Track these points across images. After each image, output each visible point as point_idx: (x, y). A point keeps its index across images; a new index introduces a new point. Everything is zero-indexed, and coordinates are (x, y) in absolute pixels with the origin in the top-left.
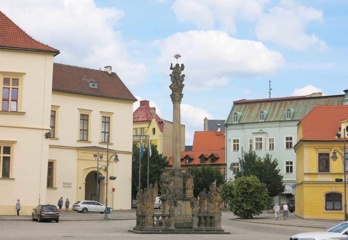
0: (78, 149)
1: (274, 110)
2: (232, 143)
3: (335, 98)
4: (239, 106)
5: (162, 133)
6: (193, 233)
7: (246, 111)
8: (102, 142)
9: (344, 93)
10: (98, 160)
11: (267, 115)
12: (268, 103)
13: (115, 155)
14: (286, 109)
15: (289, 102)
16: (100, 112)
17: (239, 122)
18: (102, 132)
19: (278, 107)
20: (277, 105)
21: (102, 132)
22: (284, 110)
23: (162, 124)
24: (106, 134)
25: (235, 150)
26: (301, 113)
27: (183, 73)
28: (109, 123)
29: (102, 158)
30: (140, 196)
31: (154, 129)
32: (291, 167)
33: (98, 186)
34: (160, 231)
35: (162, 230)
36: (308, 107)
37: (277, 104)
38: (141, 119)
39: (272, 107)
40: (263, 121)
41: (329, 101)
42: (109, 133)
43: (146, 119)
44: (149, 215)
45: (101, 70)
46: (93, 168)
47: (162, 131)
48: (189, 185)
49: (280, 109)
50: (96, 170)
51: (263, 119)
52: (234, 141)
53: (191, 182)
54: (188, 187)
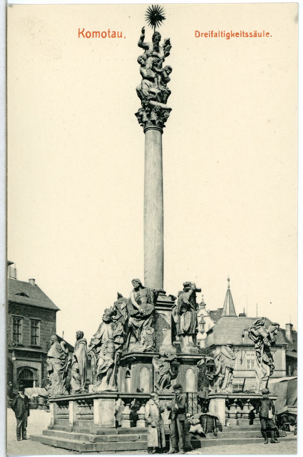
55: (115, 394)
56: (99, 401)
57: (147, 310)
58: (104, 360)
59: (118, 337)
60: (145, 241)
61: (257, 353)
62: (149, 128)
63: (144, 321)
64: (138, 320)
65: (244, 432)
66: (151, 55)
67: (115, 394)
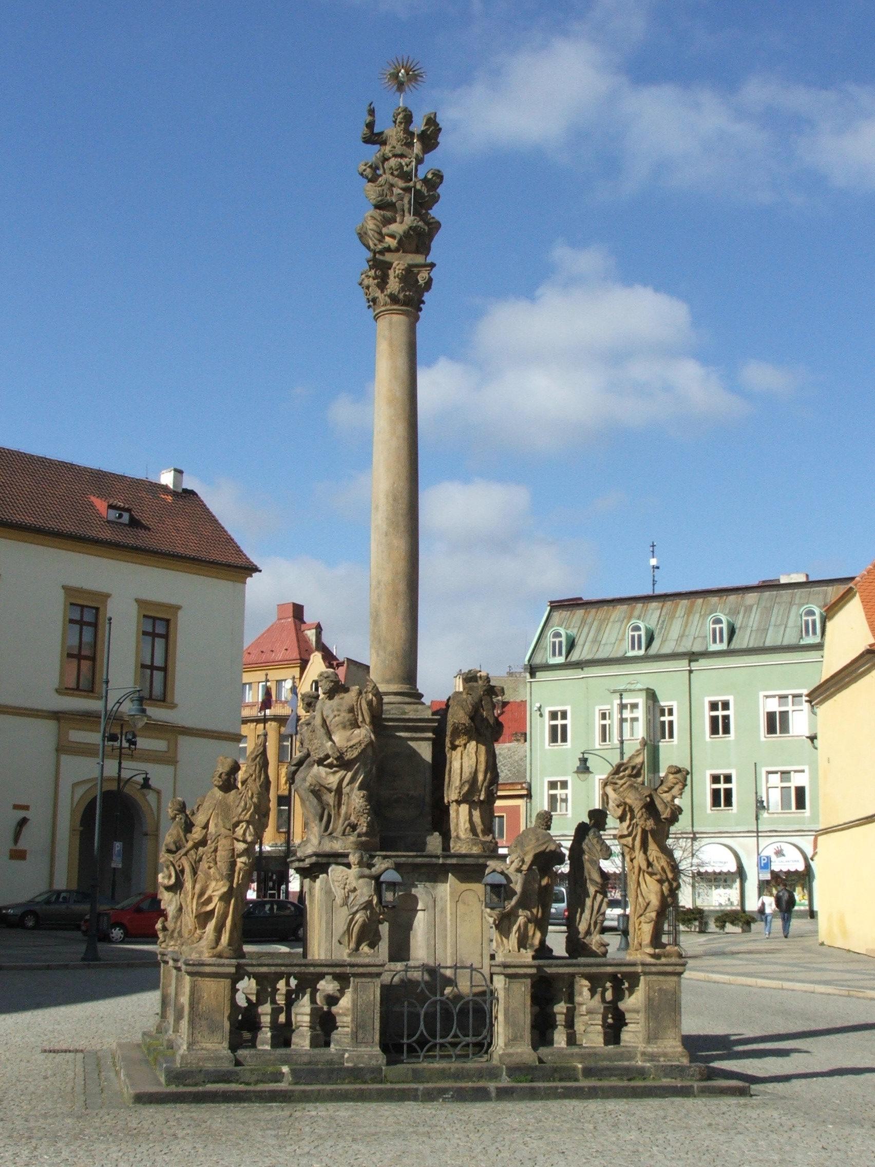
0: (56, 716)
2: (547, 722)
4: (565, 614)
7: (586, 630)
10: (121, 754)
12: (654, 605)
14: (710, 619)
15: (714, 600)
22: (700, 622)
24: (155, 672)
25: (557, 741)
26: (754, 628)
28: (166, 637)
29: (133, 747)
32: (728, 792)
34: (277, 1077)
35: (293, 1071)
36: (775, 611)
38: (280, 657)
39: (663, 613)
40: (642, 652)
42: (164, 669)
52: (554, 716)
55: (229, 965)
56: (222, 984)
57: (351, 747)
58: (813, 742)
59: (241, 825)
60: (263, 634)
61: (625, 847)
62: (380, 313)
63: (342, 773)
64: (332, 771)
65: (626, 1063)
66: (390, 155)
67: (229, 965)
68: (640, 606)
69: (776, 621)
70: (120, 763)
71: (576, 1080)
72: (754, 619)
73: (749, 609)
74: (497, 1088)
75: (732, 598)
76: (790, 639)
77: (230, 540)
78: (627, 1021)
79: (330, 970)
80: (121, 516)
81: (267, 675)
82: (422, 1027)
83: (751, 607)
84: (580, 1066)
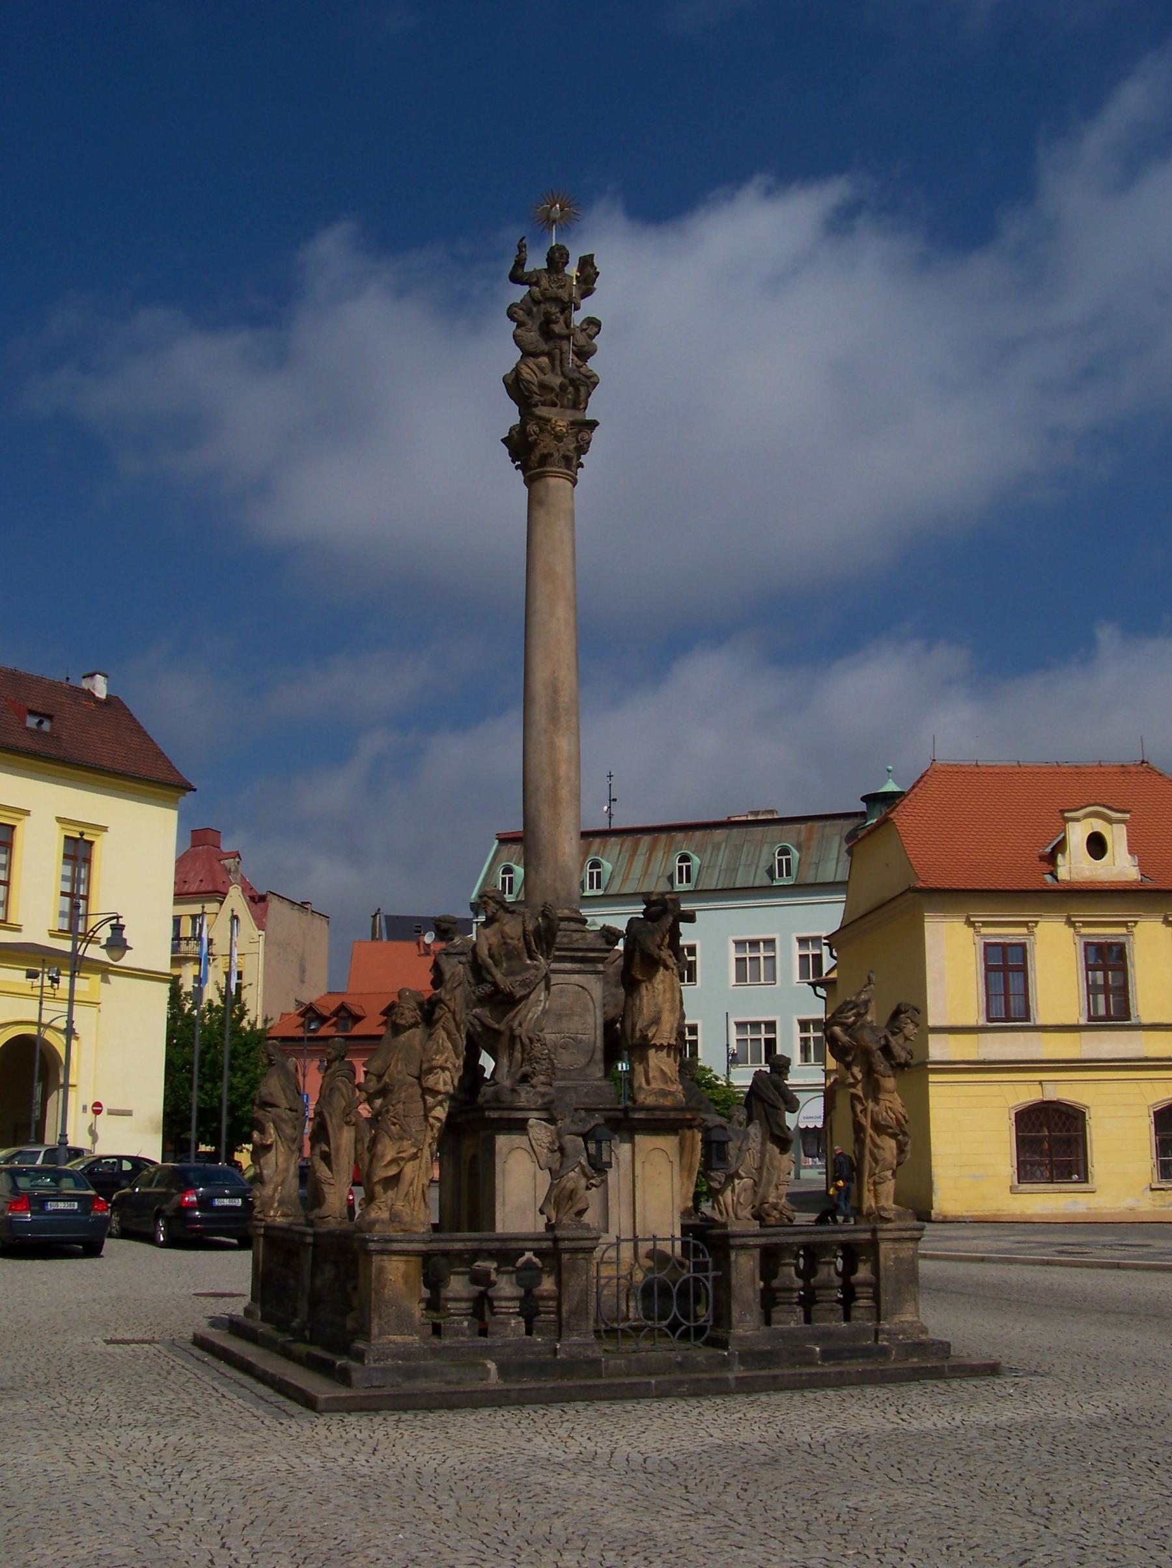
1: (632, 864)
3: (828, 823)
5: (261, 932)
6: (747, 1387)
8: (60, 931)
9: (862, 807)
11: (611, 878)
13: (114, 922)
15: (679, 836)
16: (59, 820)
17: (517, 896)
18: (63, 894)
19: (645, 849)
20: (641, 845)
21: (63, 894)
22: (663, 864)
23: (262, 905)
27: (588, 308)
29: (56, 985)
30: (284, 1103)
31: (235, 918)
33: (38, 1091)
37: (642, 842)
39: (624, 850)
40: (600, 892)
41: (733, 870)
43: (210, 888)
44: (396, 1246)
45: (70, 683)
46: (16, 1027)
47: (261, 926)
48: (656, 1021)
49: (653, 859)
50: (32, 1030)
51: (598, 887)
53: (668, 995)
54: (653, 1030)
68: (597, 841)
69: (710, 862)
70: (41, 1003)
71: (812, 1364)
72: (723, 858)
73: (717, 847)
74: (737, 1378)
75: (698, 834)
76: (762, 880)
77: (160, 754)
78: (857, 1295)
79: (529, 1245)
80: (41, 722)
81: (203, 907)
82: (675, 1309)
83: (719, 844)
84: (818, 1349)
